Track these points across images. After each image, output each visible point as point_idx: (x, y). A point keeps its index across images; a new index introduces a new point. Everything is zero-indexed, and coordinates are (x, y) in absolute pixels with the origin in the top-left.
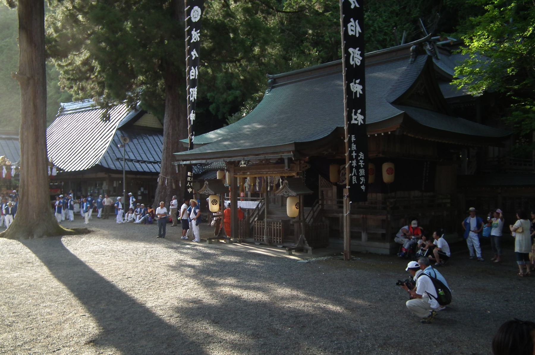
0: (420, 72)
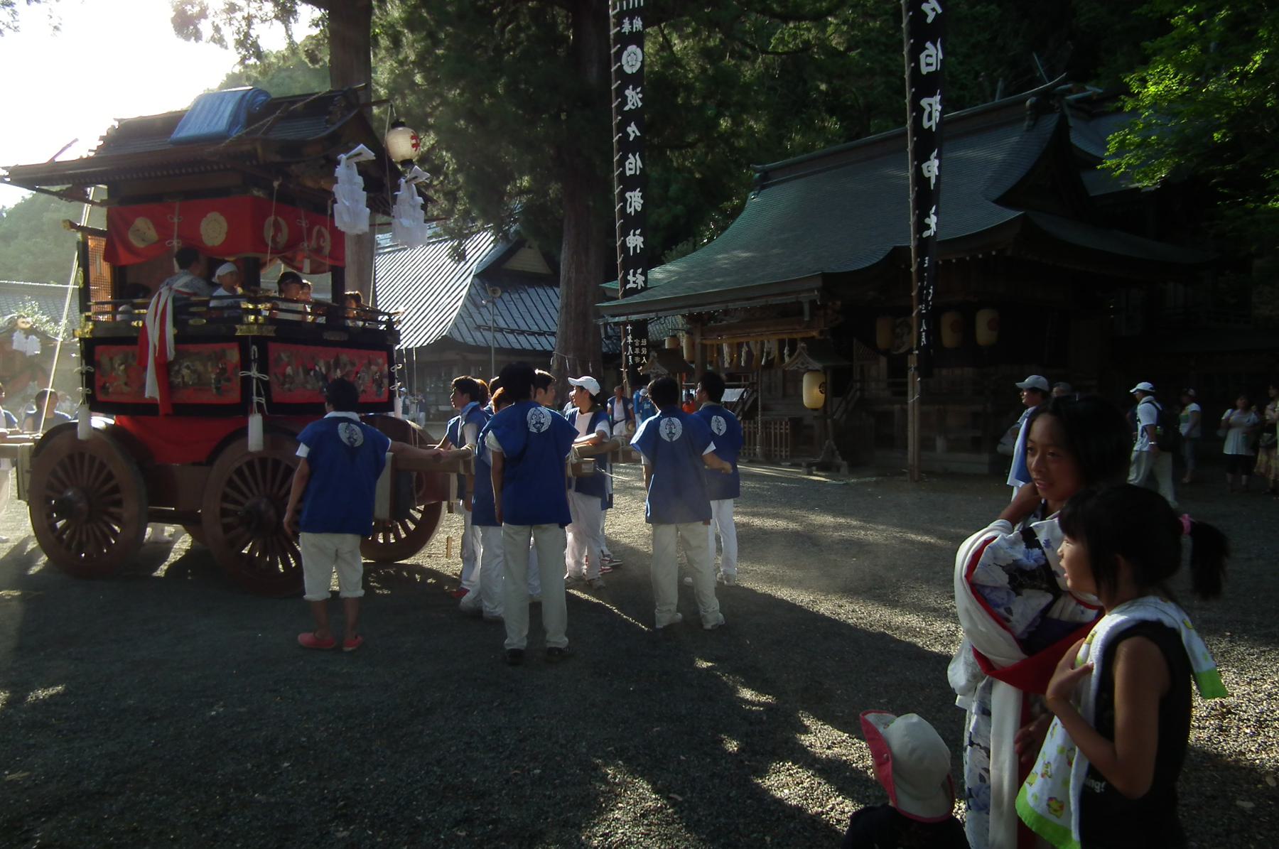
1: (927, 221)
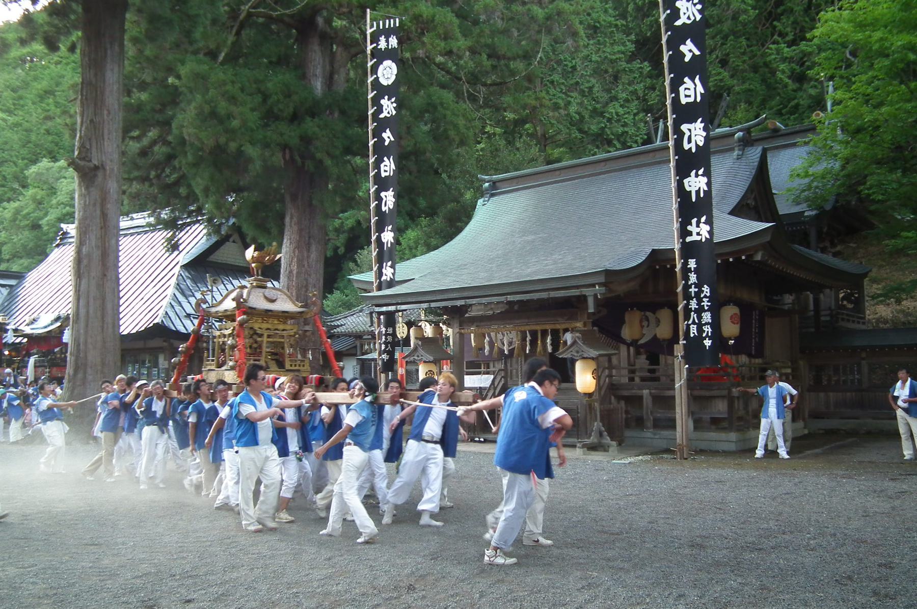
0: (754, 171)
1: (689, 228)
